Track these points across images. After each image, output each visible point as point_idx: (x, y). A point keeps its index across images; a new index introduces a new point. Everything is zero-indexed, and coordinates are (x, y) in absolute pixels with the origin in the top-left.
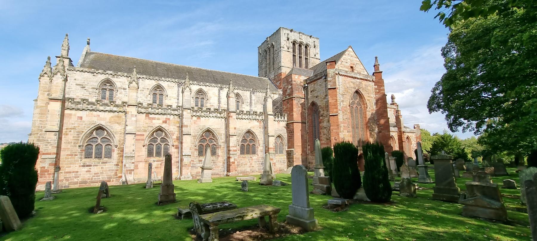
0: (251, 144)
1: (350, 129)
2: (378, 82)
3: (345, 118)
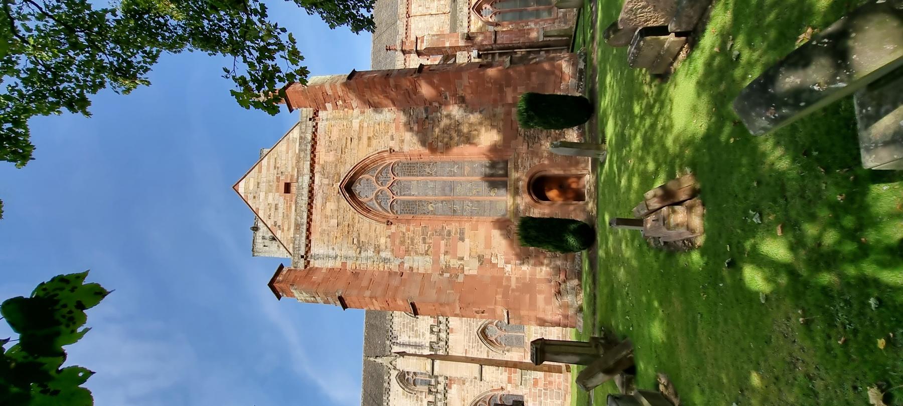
3: (422, 247)
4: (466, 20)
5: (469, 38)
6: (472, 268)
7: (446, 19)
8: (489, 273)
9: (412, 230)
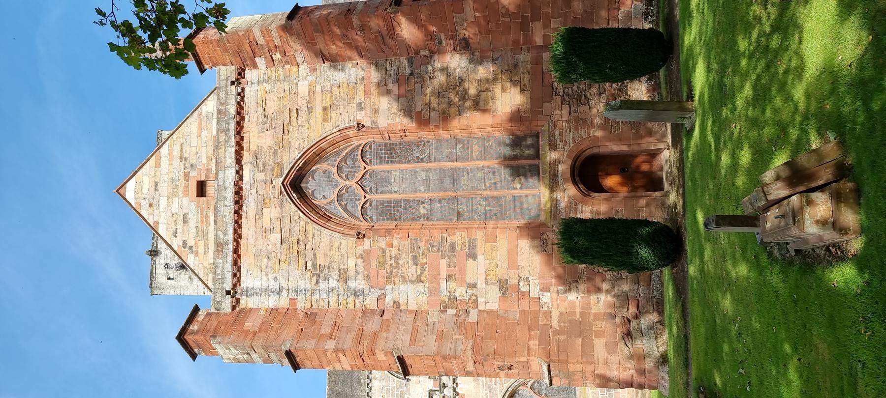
1: (458, 238)
2: (238, 53)
3: (412, 271)
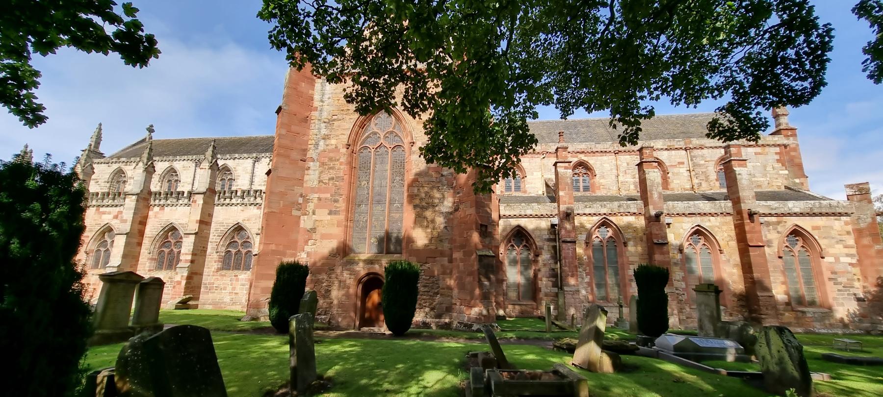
0: (244, 251)
3: (325, 177)
4: (592, 211)
5: (568, 216)
6: (306, 223)
7: (613, 192)
8: (301, 238)
9: (341, 168)
